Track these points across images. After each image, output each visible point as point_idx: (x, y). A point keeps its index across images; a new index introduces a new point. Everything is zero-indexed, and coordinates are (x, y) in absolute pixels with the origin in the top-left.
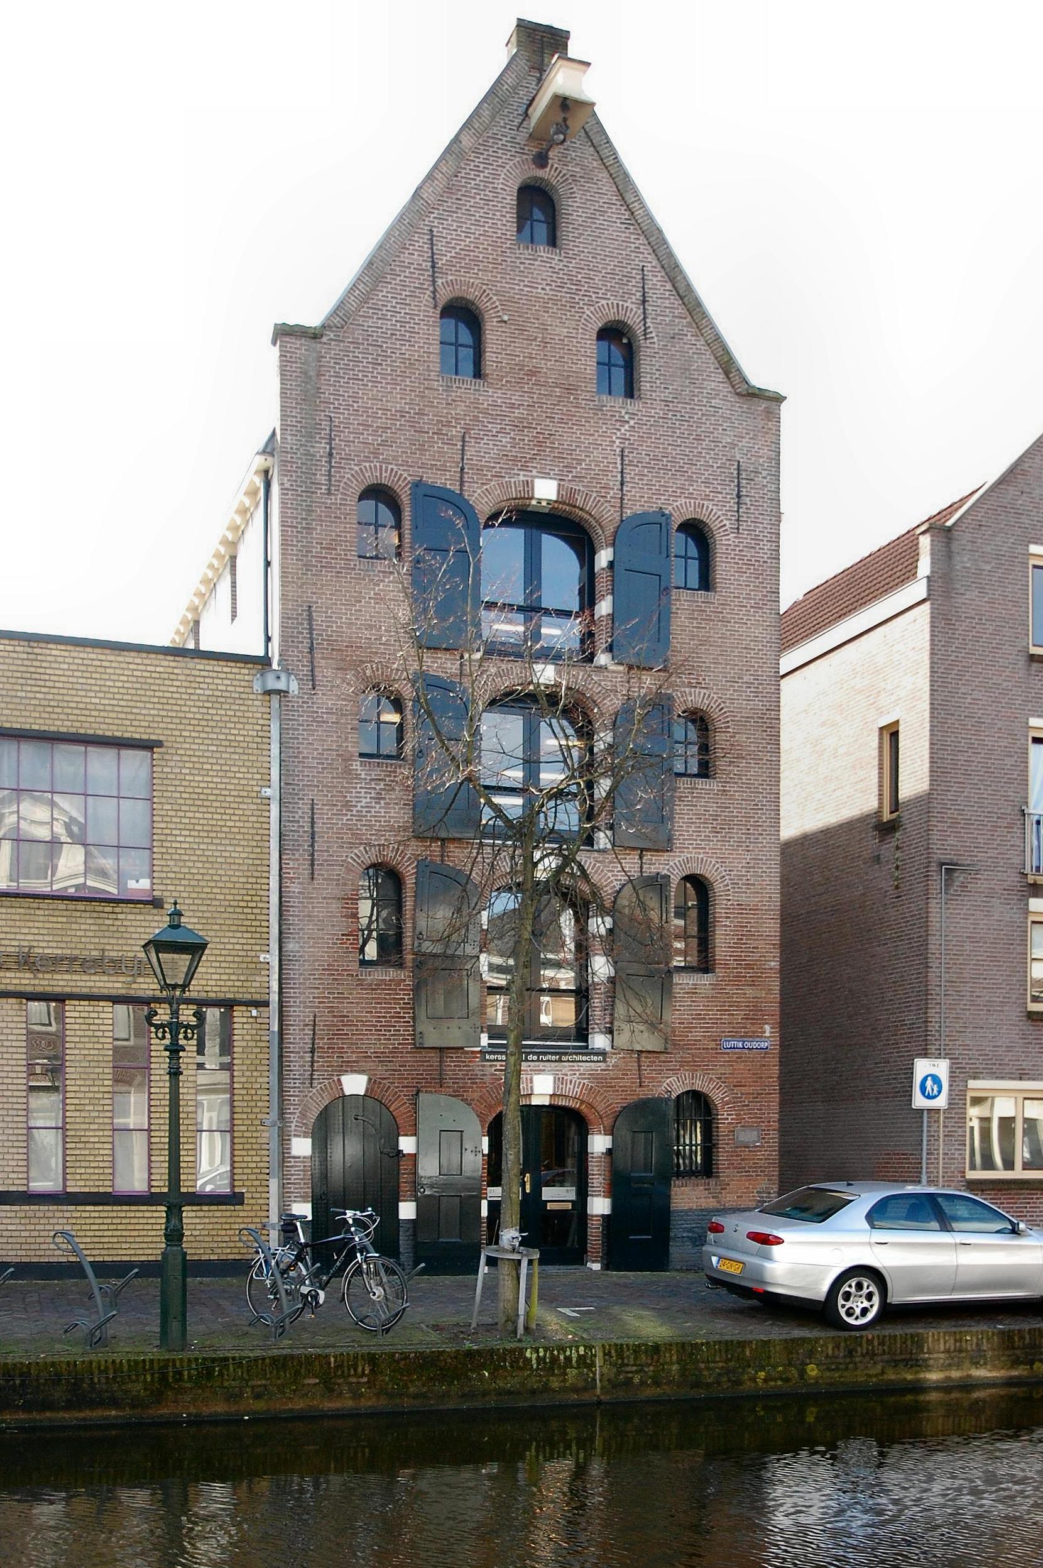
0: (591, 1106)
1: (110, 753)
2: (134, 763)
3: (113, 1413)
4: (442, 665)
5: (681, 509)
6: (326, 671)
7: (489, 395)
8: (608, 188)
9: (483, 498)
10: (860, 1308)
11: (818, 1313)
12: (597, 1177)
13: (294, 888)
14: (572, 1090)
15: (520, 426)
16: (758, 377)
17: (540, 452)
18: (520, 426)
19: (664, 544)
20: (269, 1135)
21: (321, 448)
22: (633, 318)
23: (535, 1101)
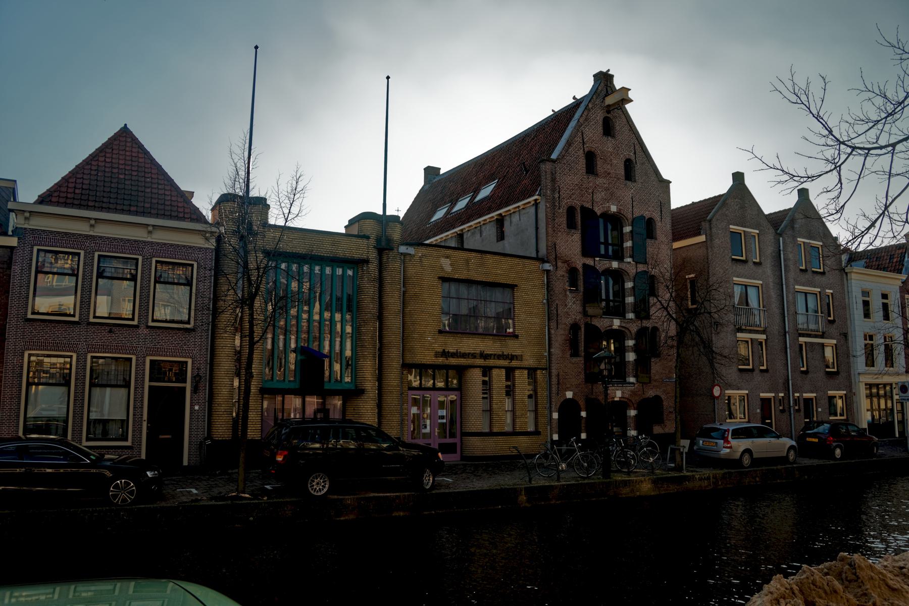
0: (630, 400)
1: (501, 289)
2: (508, 291)
3: (402, 514)
4: (589, 262)
5: (647, 215)
6: (559, 264)
7: (599, 181)
8: (625, 120)
9: (598, 211)
10: (746, 460)
11: (737, 463)
12: (631, 423)
13: (553, 332)
14: (626, 396)
15: (607, 189)
16: (665, 176)
17: (611, 197)
18: (607, 189)
19: (181, 326)
20: (547, 412)
21: (557, 195)
22: (633, 158)
23: (616, 399)
